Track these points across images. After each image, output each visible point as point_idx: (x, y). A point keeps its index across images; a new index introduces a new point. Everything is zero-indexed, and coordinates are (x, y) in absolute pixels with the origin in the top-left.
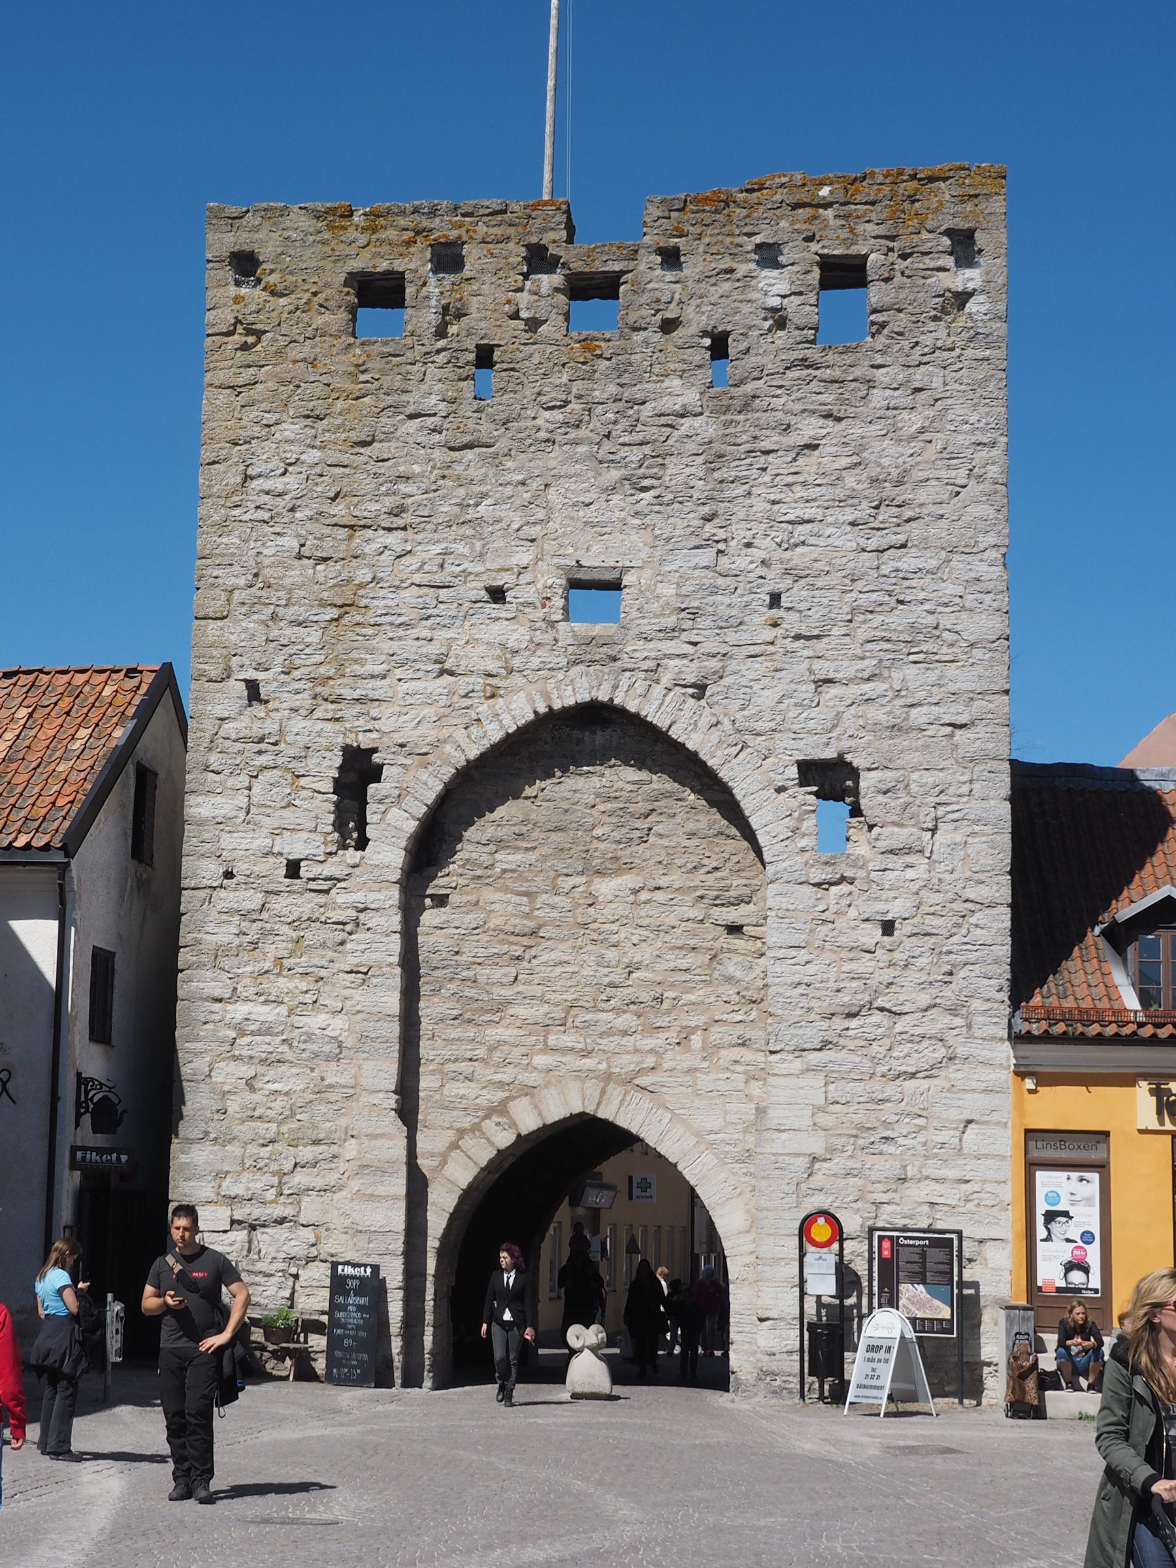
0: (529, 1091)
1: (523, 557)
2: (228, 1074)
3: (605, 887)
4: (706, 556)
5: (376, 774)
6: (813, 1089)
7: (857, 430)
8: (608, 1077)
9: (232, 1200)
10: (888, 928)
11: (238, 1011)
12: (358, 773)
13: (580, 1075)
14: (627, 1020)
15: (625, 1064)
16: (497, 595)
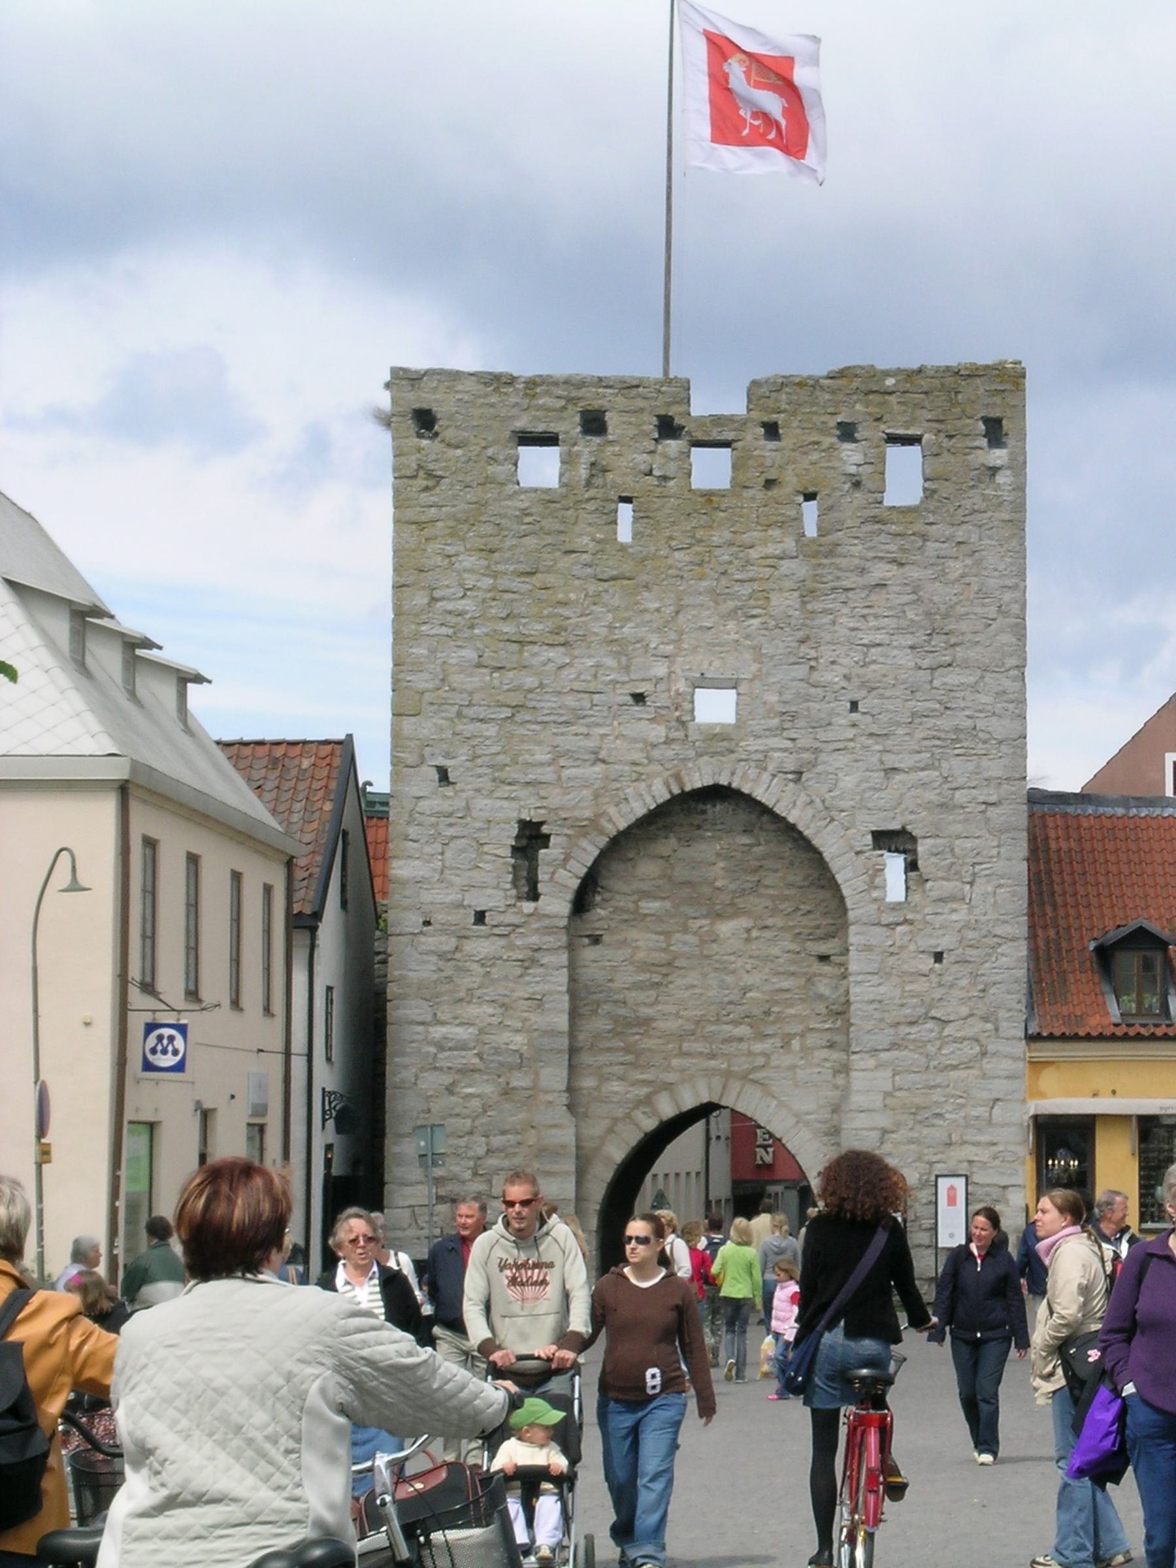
0: (668, 1087)
1: (660, 670)
2: (431, 1082)
3: (725, 928)
4: (801, 671)
5: (544, 840)
6: (883, 1079)
7: (914, 573)
8: (728, 1075)
9: (438, 1181)
10: (938, 957)
11: (437, 1032)
12: (531, 838)
13: (709, 1073)
14: (743, 1030)
15: (741, 1065)
16: (639, 698)
